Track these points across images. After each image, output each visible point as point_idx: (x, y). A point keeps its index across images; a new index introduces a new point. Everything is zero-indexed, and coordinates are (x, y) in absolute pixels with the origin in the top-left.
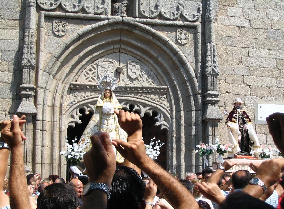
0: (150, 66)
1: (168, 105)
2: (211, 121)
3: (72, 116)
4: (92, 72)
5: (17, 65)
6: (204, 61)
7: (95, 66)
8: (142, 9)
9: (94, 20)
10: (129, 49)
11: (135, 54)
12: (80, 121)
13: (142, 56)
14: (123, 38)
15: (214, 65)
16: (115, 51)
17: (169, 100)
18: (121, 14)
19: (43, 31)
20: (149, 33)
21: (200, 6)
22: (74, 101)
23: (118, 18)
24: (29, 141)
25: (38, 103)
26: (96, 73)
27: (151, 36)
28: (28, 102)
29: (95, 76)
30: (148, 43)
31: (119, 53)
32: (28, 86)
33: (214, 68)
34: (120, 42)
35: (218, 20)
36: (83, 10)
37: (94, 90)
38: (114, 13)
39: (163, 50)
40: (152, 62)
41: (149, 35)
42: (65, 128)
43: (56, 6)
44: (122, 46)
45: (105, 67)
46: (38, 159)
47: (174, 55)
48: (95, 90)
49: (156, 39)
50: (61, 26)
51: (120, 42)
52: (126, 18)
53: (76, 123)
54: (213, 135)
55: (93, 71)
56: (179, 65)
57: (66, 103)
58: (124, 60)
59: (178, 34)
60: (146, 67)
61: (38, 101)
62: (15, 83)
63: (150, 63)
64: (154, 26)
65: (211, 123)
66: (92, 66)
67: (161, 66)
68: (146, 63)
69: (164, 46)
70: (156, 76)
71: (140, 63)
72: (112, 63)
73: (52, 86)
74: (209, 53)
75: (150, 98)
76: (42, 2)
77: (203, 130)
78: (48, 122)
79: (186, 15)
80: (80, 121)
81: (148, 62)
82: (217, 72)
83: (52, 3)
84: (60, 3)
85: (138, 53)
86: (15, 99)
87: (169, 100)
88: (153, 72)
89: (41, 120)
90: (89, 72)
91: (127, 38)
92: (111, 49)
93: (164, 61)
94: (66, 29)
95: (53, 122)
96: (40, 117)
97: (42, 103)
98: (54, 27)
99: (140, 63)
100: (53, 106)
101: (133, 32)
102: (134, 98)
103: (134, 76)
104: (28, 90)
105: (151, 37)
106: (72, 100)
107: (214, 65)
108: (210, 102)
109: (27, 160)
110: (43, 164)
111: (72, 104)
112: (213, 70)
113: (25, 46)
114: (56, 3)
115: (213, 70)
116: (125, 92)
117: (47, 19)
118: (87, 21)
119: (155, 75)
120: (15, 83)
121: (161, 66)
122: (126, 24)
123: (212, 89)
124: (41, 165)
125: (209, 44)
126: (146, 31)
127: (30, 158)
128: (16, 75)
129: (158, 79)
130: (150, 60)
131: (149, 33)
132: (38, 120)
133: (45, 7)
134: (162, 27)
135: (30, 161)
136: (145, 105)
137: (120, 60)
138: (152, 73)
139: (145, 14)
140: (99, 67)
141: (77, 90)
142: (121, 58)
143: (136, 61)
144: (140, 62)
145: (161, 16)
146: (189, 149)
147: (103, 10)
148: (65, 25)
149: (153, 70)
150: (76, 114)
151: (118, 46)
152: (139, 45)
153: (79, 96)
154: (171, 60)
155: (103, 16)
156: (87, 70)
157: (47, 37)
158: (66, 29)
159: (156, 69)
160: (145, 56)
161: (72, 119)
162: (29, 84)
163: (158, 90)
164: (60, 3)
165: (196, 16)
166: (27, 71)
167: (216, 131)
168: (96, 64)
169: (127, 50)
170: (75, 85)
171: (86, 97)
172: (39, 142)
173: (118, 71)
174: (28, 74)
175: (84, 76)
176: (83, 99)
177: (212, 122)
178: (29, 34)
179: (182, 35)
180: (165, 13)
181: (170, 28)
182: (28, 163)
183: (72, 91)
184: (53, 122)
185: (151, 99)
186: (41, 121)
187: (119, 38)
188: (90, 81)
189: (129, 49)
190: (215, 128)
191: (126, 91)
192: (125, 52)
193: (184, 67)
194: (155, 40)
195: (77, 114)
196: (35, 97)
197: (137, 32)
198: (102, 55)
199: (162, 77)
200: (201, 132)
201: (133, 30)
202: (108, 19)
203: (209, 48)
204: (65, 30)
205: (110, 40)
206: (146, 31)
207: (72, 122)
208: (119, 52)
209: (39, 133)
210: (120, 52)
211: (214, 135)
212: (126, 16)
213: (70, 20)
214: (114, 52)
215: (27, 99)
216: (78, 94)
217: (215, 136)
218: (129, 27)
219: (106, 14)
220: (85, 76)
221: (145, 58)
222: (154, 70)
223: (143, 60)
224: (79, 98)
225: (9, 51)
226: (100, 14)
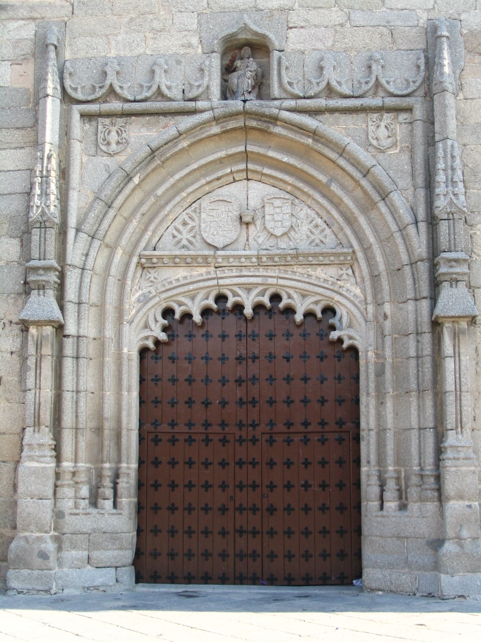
0: (315, 206)
1: (358, 291)
2: (449, 322)
3: (146, 326)
4: (189, 227)
5: (25, 223)
8: (285, 80)
9: (184, 112)
10: (266, 171)
11: (281, 180)
12: (163, 336)
14: (250, 148)
15: (453, 192)
16: (237, 179)
18: (243, 94)
19: (77, 148)
20: (304, 130)
21: (419, 61)
23: (236, 105)
24: (44, 381)
25: (67, 300)
26: (197, 228)
27: (309, 137)
28: (42, 297)
29: (194, 237)
30: (305, 153)
31: (246, 181)
32: (42, 263)
33: (453, 197)
34: (246, 156)
35: (466, 88)
36: (159, 94)
37: (191, 265)
38: (228, 95)
39: (338, 166)
40: (317, 196)
41: (304, 137)
42: (131, 352)
43: (104, 90)
44: (250, 166)
45: (215, 215)
46: (68, 419)
48: (193, 265)
49: (323, 144)
52: (254, 104)
54: (455, 357)
55: (189, 224)
56: (377, 198)
57: (132, 298)
58: (257, 196)
59: (372, 128)
60: (306, 208)
63: (313, 199)
64: (316, 114)
65: (449, 327)
66: (187, 214)
67: (337, 204)
68: (304, 198)
69: (340, 158)
70: (330, 228)
71: (293, 200)
73: (98, 260)
74: (441, 165)
75: (314, 278)
77: (433, 344)
78: (95, 339)
79: (388, 82)
81: (309, 196)
82: (460, 206)
84: (111, 85)
87: (359, 280)
88: (321, 218)
89: (73, 336)
90: (181, 228)
91: (259, 146)
92: (227, 175)
95: (100, 340)
96: (71, 329)
97: (77, 298)
98: (99, 136)
99: (293, 200)
100: (101, 306)
101: (269, 130)
102: (279, 280)
103: (278, 232)
104: (41, 272)
105: (310, 141)
106: (145, 291)
107: (453, 192)
108: (446, 278)
109: (41, 420)
110: (78, 431)
111: (145, 300)
113: (36, 179)
115: (451, 203)
116: (258, 267)
117: (86, 121)
118: (170, 117)
119: (328, 225)
121: (337, 204)
122: (253, 116)
124: (74, 433)
125: (440, 145)
127: (47, 416)
128: (24, 243)
129: (335, 234)
130: (311, 192)
131: (304, 130)
133: (80, 96)
134: (333, 115)
135: (48, 423)
136: (248, 288)
138: (319, 221)
139: (293, 88)
140: (203, 215)
142: (250, 192)
144: (292, 198)
145: (330, 91)
146: (407, 391)
147: (201, 90)
148: (123, 129)
150: (153, 319)
151: (242, 166)
152: (285, 159)
153: (159, 280)
154: (359, 188)
155: (200, 104)
156: (177, 224)
157: (85, 159)
159: (328, 212)
160: (300, 185)
161: (147, 333)
162: (44, 259)
163: (332, 258)
164: (111, 85)
165: (411, 84)
166: (40, 233)
167: (461, 346)
169: (263, 174)
170: (149, 259)
171: (174, 282)
172: (69, 383)
174: (42, 239)
175: (171, 237)
176: (168, 287)
177: (453, 325)
178: (43, 156)
179: (381, 129)
180: (339, 83)
181: (354, 115)
182: (43, 427)
183: (145, 270)
184: (100, 340)
185: (318, 278)
186: (75, 338)
187: (242, 148)
188: (184, 247)
189: (266, 171)
190: (461, 338)
192: (258, 177)
193: (388, 203)
194: (320, 145)
195: (156, 321)
196: (61, 288)
197: (277, 130)
198: (207, 188)
199: (342, 229)
200: (429, 349)
201: (269, 128)
202: (212, 109)
203: (440, 153)
205: (222, 154)
206: (299, 128)
207: (147, 338)
209: (68, 364)
210: (248, 179)
211: (457, 355)
212: (254, 99)
213: (133, 117)
214: (235, 181)
215: (41, 292)
217: (459, 356)
218: (260, 123)
219: (209, 99)
220: (174, 237)
222: (324, 214)
223: (298, 193)
224: (159, 286)
225: (194, 202)
226: (194, 100)
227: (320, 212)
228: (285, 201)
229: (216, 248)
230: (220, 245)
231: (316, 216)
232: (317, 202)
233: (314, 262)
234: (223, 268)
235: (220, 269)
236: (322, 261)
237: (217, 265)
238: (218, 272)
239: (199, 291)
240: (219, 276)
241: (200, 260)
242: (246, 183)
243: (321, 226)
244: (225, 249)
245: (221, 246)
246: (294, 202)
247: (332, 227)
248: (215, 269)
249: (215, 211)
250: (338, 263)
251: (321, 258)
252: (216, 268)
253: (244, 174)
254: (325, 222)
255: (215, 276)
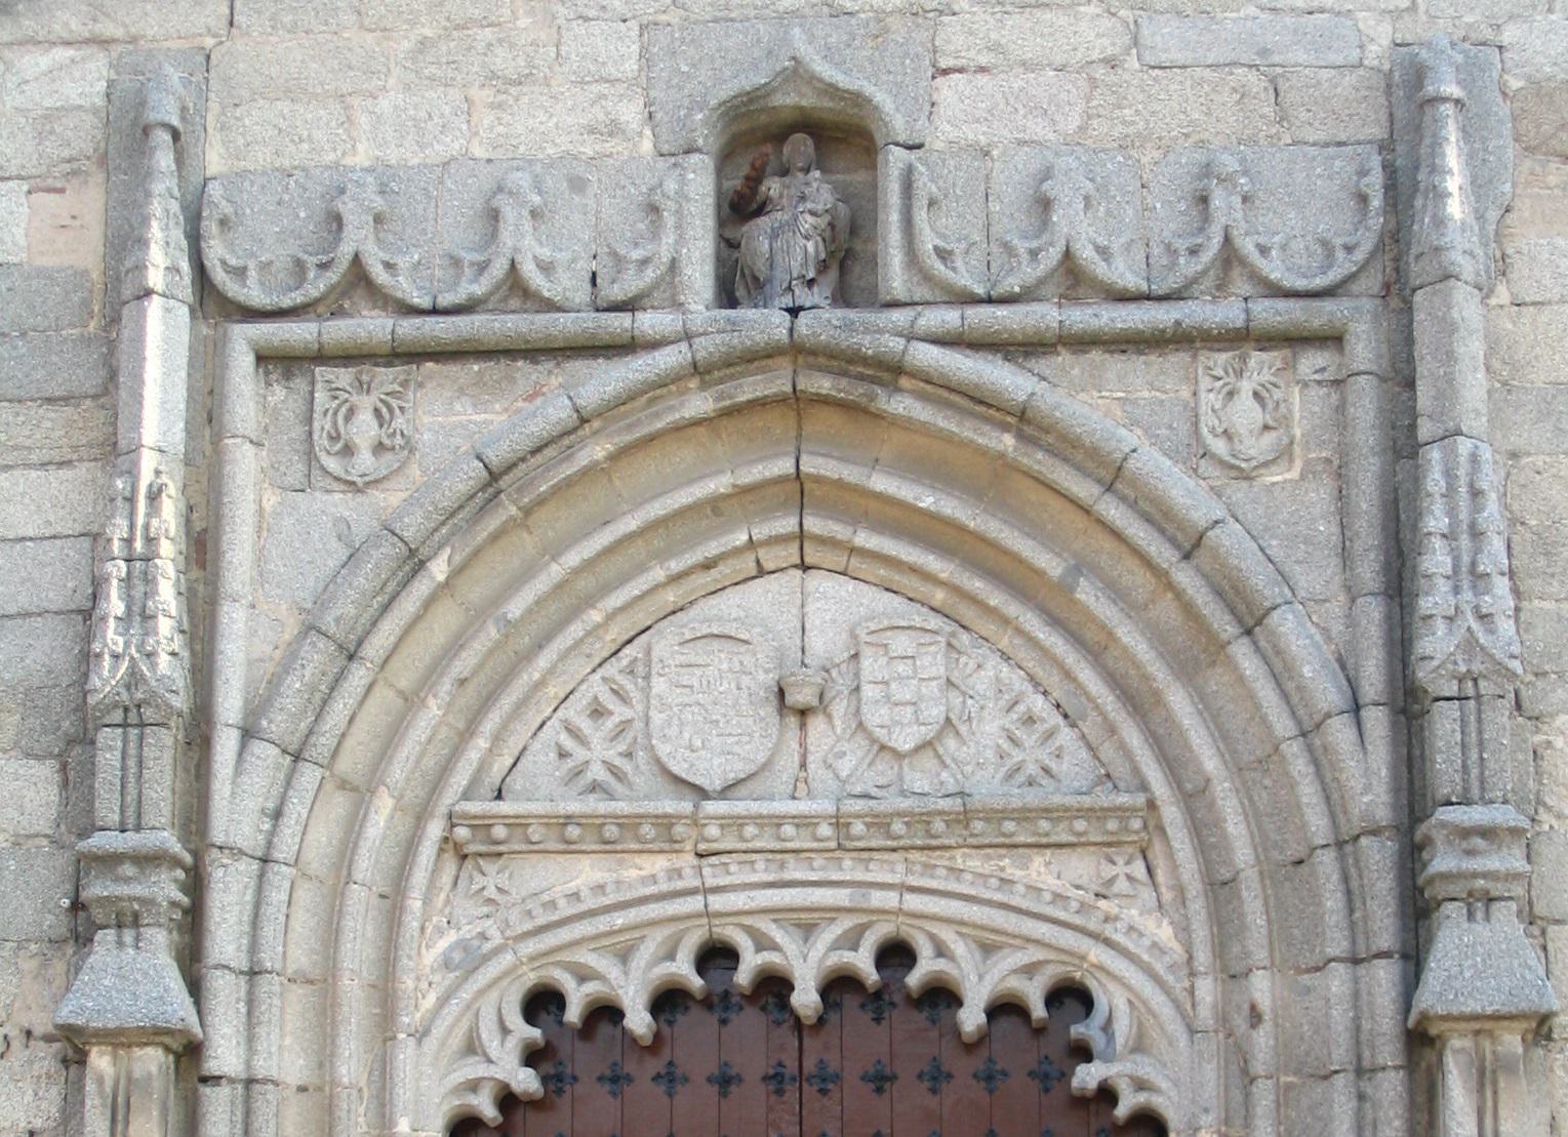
0: (1023, 654)
1: (1165, 933)
2: (1463, 1035)
3: (472, 1047)
5: (75, 710)
6: (1399, 585)
7: (625, 682)
8: (928, 241)
12: (526, 1081)
13: (957, 582)
15: (1476, 609)
16: (769, 565)
17: (1163, 890)
18: (790, 288)
19: (244, 464)
20: (990, 406)
21: (1366, 180)
22: (483, 936)
23: (765, 323)
26: (639, 725)
27: (1005, 427)
28: (131, 951)
29: (629, 755)
30: (992, 482)
31: (799, 573)
33: (1475, 625)
34: (799, 491)
36: (515, 286)
38: (740, 292)
39: (1102, 523)
40: (1032, 622)
43: (333, 276)
44: (813, 524)
47: (1187, 556)
48: (625, 846)
49: (1050, 451)
50: (365, 417)
51: (799, 491)
52: (824, 322)
53: (508, 1100)
55: (611, 713)
56: (1226, 627)
57: (426, 958)
58: (834, 621)
60: (993, 661)
61: (208, 943)
62: (63, 827)
63: (1019, 631)
64: (1027, 355)
66: (604, 679)
67: (1097, 648)
68: (989, 628)
69: (1108, 497)
70: (1073, 725)
72: (745, 647)
73: (312, 832)
74: (1436, 521)
75: (1020, 888)
76: (233, 262)
78: (302, 1089)
79: (1264, 250)
80: (526, 1081)
81: (1005, 621)
82: (1499, 655)
83: (304, 262)
85: (932, 562)
86: (65, 941)
87: (1168, 896)
88: (1045, 693)
89: (232, 1081)
90: (585, 725)
91: (840, 459)
92: (737, 552)
93: (1114, 609)
94: (402, 434)
96: (225, 1056)
99: (953, 634)
100: (323, 983)
102: (908, 897)
104: (128, 870)
105: (1008, 441)
106: (468, 931)
107: (1476, 609)
108: (1455, 889)
111: (468, 961)
112: (1470, 644)
113: (109, 567)
114: (325, 259)
115: (1470, 644)
116: (838, 854)
117: (274, 377)
118: (550, 365)
119: (1066, 716)
120: (63, 827)
121: (1097, 648)
123: (1466, 790)
125: (1435, 454)
126: (972, 398)
131: (990, 406)
132: (215, 1080)
133: (254, 294)
136: (806, 924)
137: (807, 626)
138: (1038, 704)
139: (954, 269)
140: (659, 685)
141: (500, 855)
143: (918, 622)
145: (1073, 278)
147: (650, 274)
148: (394, 403)
149: (1045, 683)
150: (494, 1026)
151: (787, 524)
152: (927, 501)
155: (649, 322)
157: (271, 500)
158: (402, 434)
159: (1068, 675)
160: (977, 585)
161: (475, 1069)
162: (138, 828)
163: (1080, 825)
165: (1340, 255)
167: (1502, 1113)
168: (630, 671)
169: (853, 550)
170: (482, 826)
171: (562, 903)
173: (790, 700)
174: (132, 763)
175: (553, 755)
176: (541, 921)
177: (1477, 1044)
180: (1104, 252)
181: (1152, 358)
183: (469, 864)
186: (240, 1087)
187: (785, 466)
189: (865, 539)
191: (848, 844)
192: (838, 560)
194: (1040, 455)
195: (505, 1031)
197: (901, 405)
198: (671, 597)
199: (1112, 730)
200: (1397, 1123)
201: (872, 398)
202: (688, 336)
203: (1435, 481)
204: (399, 437)
205: (719, 484)
207: (473, 1086)
208: (795, 566)
210: (805, 567)
212: (824, 303)
213: (430, 365)
214: (761, 572)
215: (128, 936)
216: (504, 883)
218: (844, 382)
219: (677, 305)
220: (563, 754)
221: (982, 596)
222: (1052, 680)
223: (968, 613)
224: (514, 916)
226: (628, 306)
227: (1039, 672)
228: (928, 638)
229: (702, 793)
230: (713, 783)
231: (1028, 687)
232: (1033, 642)
233: (1021, 839)
234: (724, 859)
235: (714, 860)
236: (1047, 835)
237: (702, 847)
238: (707, 871)
239: (645, 932)
240: (710, 882)
241: (647, 830)
242: (798, 581)
243: (1043, 720)
244: (729, 794)
245: (718, 785)
246: (954, 642)
247: (1080, 723)
248: (695, 861)
249: (698, 672)
250: (1099, 839)
251: (1044, 825)
252: (700, 856)
253: (794, 548)
254: (1058, 706)
255: (696, 883)
